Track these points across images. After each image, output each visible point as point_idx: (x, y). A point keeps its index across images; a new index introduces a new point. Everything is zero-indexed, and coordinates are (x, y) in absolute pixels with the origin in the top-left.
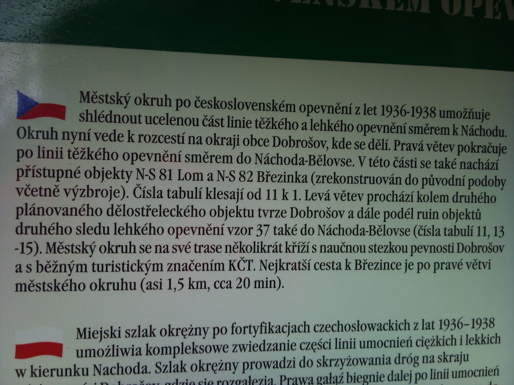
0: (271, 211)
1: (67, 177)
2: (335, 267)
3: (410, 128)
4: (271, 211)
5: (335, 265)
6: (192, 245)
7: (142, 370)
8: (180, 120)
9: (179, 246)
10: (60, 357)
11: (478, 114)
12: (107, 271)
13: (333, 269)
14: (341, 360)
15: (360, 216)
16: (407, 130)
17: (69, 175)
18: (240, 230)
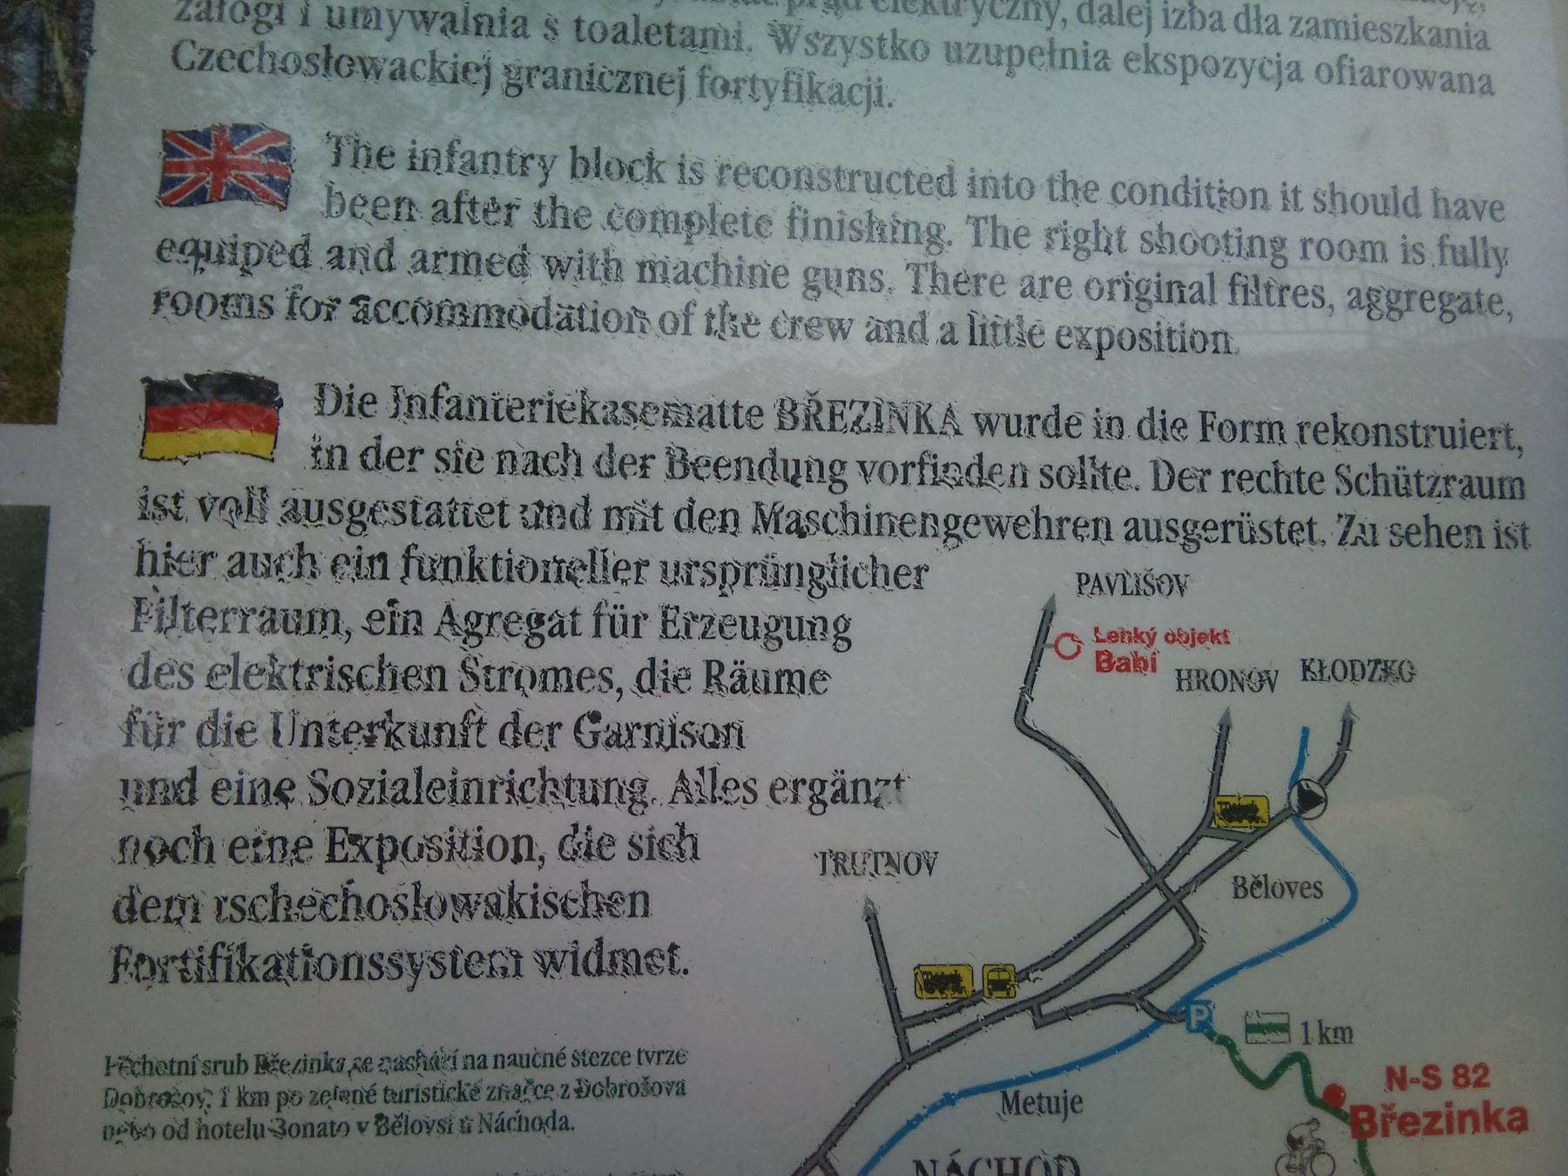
0: (659, 1054)
1: (1341, 82)
2: (422, 515)
3: (1042, 470)
4: (659, 1054)
5: (421, 509)
6: (380, 1089)
7: (427, 514)
8: (745, 465)
9: (411, 955)
10: (53, 529)
11: (1053, 1101)
12: (493, 801)
13: (415, 523)
14: (1243, 61)
15: (1086, 16)
16: (199, 1068)
17: (1160, 199)
18: (1368, 675)
